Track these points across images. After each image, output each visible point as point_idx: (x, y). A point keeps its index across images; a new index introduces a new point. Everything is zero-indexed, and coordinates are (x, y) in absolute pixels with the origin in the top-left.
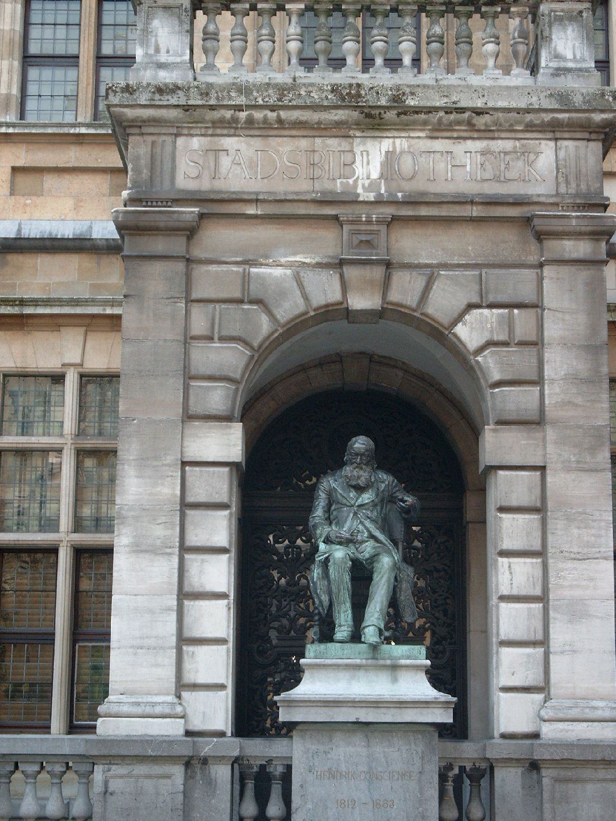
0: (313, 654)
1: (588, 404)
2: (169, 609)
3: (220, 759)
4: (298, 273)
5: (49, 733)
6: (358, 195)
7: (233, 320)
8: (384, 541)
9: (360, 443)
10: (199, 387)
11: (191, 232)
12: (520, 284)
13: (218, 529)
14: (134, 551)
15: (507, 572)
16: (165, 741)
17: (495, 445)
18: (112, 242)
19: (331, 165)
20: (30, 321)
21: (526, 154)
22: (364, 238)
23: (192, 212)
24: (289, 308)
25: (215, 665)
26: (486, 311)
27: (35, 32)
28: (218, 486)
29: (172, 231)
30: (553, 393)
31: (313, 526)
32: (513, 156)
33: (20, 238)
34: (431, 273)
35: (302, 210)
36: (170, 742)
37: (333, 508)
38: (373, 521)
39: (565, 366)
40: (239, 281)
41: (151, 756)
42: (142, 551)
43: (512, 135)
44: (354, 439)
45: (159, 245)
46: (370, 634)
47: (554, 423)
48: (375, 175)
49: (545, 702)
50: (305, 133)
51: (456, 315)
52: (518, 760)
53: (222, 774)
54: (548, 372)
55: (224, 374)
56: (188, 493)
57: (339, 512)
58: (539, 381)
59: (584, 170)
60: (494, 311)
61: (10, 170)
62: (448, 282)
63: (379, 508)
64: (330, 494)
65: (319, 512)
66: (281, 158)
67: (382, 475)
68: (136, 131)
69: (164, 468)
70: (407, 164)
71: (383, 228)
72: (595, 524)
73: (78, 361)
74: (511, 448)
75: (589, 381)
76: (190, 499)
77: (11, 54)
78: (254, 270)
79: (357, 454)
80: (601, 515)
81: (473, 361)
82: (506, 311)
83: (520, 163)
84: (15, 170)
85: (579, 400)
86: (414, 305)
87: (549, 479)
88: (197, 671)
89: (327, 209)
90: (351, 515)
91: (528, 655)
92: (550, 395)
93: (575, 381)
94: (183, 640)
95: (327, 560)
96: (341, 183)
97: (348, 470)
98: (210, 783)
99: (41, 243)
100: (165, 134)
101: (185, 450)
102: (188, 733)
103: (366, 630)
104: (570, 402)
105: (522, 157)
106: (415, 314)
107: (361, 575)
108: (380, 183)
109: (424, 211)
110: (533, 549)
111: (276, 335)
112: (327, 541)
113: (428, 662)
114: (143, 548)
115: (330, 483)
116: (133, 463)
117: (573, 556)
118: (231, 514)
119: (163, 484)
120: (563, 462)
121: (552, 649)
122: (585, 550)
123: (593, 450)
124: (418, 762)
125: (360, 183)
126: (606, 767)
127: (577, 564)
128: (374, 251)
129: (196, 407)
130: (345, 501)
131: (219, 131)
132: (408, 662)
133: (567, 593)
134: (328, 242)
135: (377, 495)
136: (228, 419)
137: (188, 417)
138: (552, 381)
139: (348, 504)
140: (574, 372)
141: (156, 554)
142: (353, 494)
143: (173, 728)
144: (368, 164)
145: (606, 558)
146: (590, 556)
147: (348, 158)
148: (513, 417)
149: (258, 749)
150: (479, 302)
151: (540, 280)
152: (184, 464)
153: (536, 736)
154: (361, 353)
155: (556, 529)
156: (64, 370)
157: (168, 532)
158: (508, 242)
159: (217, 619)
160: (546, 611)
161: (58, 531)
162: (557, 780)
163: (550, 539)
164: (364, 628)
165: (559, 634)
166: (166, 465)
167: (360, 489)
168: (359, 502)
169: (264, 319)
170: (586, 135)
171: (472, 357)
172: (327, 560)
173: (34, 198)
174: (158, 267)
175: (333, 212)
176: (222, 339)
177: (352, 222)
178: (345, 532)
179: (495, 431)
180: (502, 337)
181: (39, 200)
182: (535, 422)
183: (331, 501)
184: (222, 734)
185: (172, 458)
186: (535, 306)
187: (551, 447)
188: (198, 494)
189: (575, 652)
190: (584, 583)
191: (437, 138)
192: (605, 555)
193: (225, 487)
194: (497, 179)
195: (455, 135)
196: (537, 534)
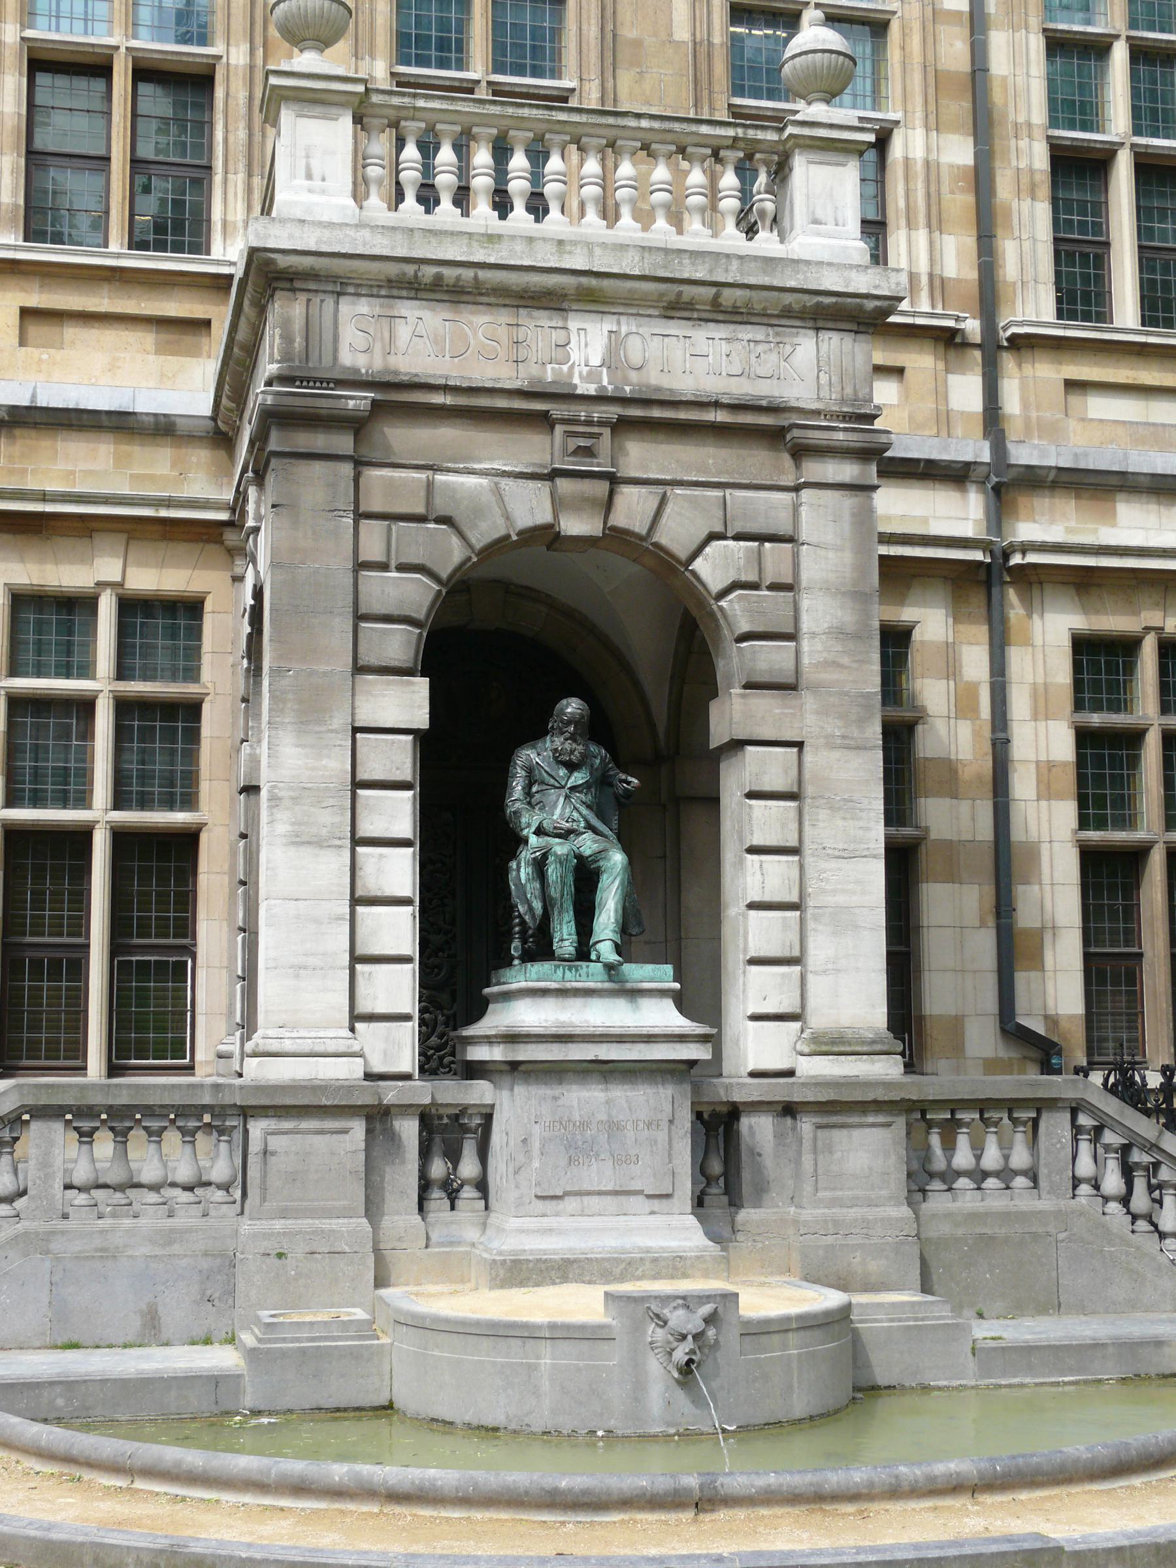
1: (855, 665)
2: (339, 918)
3: (405, 1109)
4: (496, 484)
5: (193, 1075)
6: (576, 386)
7: (418, 542)
9: (572, 707)
12: (771, 508)
13: (397, 813)
14: (293, 843)
15: (758, 873)
16: (342, 1087)
18: (162, 418)
20: (53, 523)
22: (582, 442)
23: (365, 398)
24: (484, 532)
25: (397, 989)
26: (731, 543)
28: (396, 758)
30: (812, 650)
31: (515, 812)
33: (36, 408)
35: (502, 403)
36: (348, 1088)
37: (534, 789)
38: (588, 807)
39: (828, 618)
40: (423, 493)
41: (325, 1106)
43: (765, 320)
44: (564, 702)
45: (320, 441)
46: (606, 951)
47: (815, 688)
48: (596, 361)
49: (802, 1031)
50: (501, 301)
51: (694, 546)
52: (770, 1103)
53: (409, 1130)
54: (806, 624)
55: (403, 613)
56: (359, 769)
60: (742, 543)
64: (530, 770)
69: (330, 735)
71: (607, 432)
72: (864, 814)
73: (118, 579)
74: (763, 718)
75: (857, 637)
76: (362, 775)
78: (440, 477)
80: (870, 803)
81: (714, 607)
82: (756, 544)
83: (773, 357)
84: (27, 313)
85: (845, 660)
86: (644, 532)
88: (375, 998)
89: (530, 409)
90: (562, 799)
91: (783, 975)
92: (811, 652)
93: (841, 636)
96: (553, 369)
98: (393, 1138)
100: (324, 292)
102: (369, 1076)
103: (599, 946)
104: (834, 662)
105: (776, 350)
107: (586, 876)
108: (601, 373)
109: (656, 413)
110: (788, 844)
112: (539, 832)
114: (305, 838)
115: (529, 755)
116: (290, 727)
117: (837, 853)
118: (414, 795)
119: (329, 757)
120: (826, 737)
122: (852, 847)
123: (861, 722)
124: (668, 1108)
125: (577, 369)
127: (842, 863)
128: (595, 461)
129: (369, 657)
130: (552, 781)
131: (395, 292)
133: (830, 900)
134: (534, 449)
135: (591, 774)
137: (359, 669)
138: (814, 635)
139: (557, 784)
141: (321, 847)
142: (562, 772)
143: (348, 1070)
145: (875, 857)
146: (857, 853)
148: (766, 678)
149: (452, 1092)
150: (723, 530)
151: (796, 508)
152: (356, 730)
153: (790, 1073)
154: (496, 581)
155: (818, 820)
156: (97, 590)
157: (337, 819)
158: (757, 461)
160: (802, 921)
161: (89, 807)
165: (819, 950)
166: (332, 731)
167: (572, 767)
169: (455, 540)
171: (712, 602)
173: (52, 351)
174: (318, 468)
176: (402, 568)
177: (565, 421)
179: (743, 696)
180: (752, 577)
181: (58, 355)
184: (407, 1077)
185: (340, 720)
186: (790, 540)
187: (805, 717)
188: (371, 770)
189: (838, 971)
190: (850, 887)
191: (673, 318)
192: (875, 852)
195: (695, 315)
196: (794, 826)
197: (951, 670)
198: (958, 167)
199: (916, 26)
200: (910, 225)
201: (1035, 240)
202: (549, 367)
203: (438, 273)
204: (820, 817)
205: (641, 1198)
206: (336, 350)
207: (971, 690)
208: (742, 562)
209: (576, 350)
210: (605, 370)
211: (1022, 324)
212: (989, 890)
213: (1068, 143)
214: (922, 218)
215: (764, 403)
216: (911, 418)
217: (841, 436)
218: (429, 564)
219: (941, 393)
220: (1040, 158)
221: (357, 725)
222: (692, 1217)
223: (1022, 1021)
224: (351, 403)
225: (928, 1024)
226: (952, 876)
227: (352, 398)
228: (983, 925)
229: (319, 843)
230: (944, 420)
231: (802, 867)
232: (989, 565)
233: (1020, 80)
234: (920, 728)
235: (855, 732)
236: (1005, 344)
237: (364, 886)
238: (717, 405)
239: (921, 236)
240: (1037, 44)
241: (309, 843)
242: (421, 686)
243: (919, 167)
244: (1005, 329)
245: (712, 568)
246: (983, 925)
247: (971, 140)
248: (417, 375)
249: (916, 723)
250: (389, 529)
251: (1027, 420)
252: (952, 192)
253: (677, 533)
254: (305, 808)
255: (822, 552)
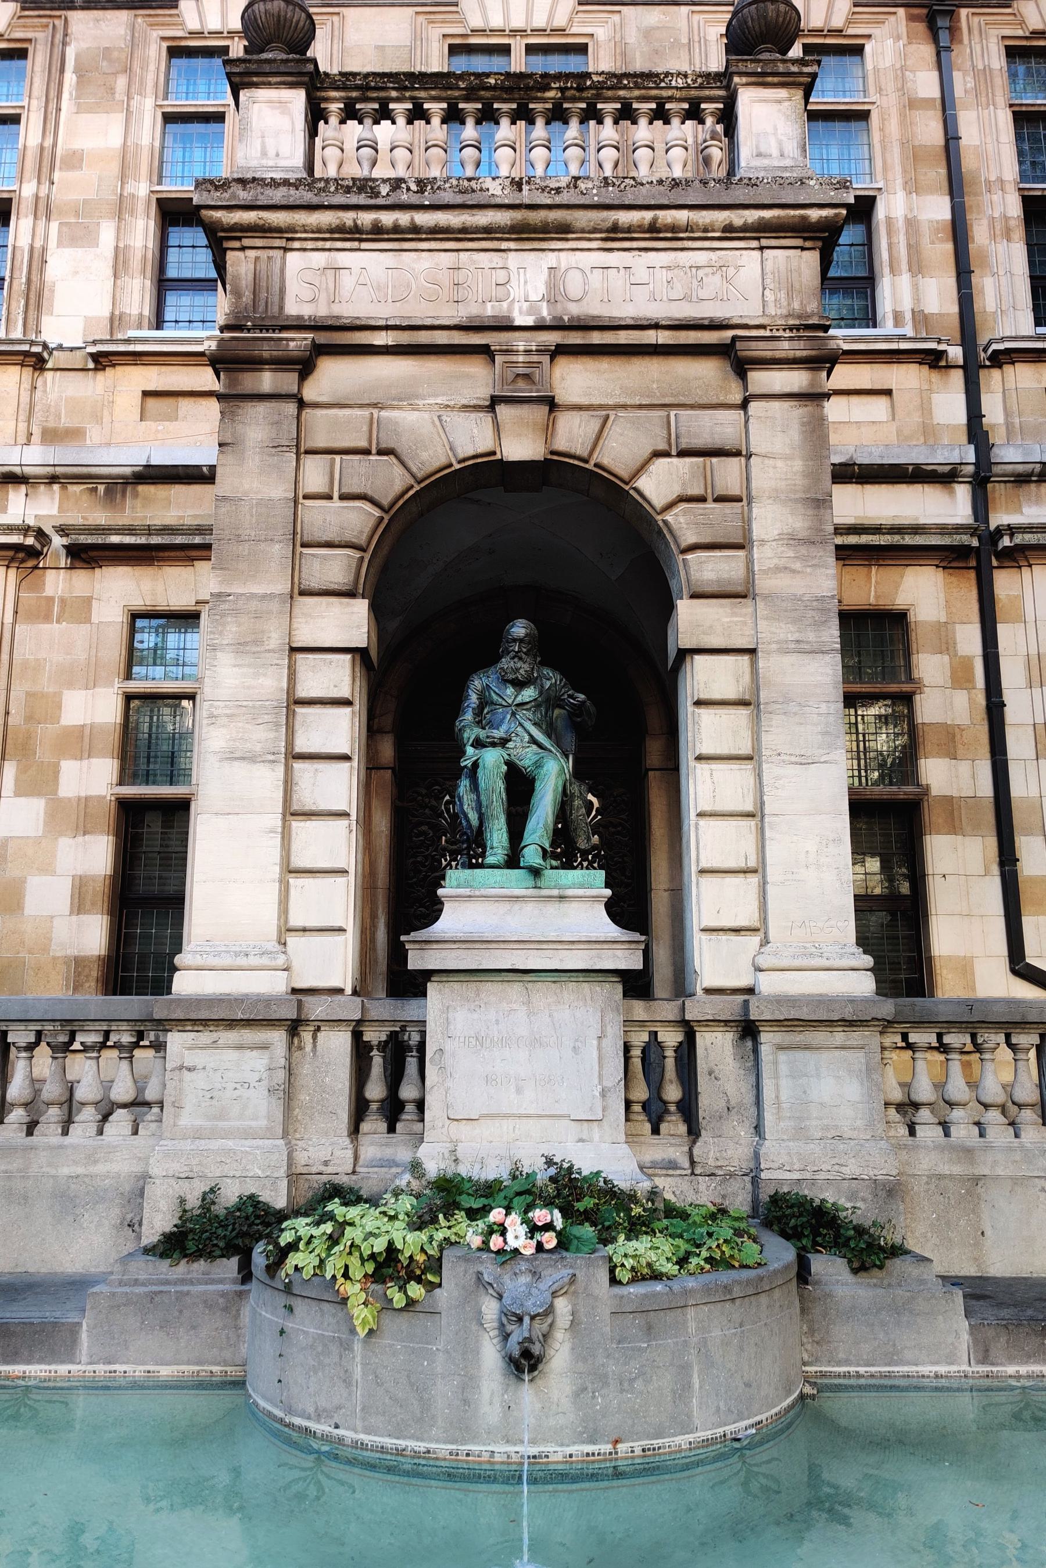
0: (456, 882)
7: (360, 473)
8: (549, 747)
10: (313, 555)
11: (305, 367)
13: (339, 730)
15: (709, 781)
17: (692, 621)
19: (480, 286)
21: (724, 269)
23: (305, 339)
25: (335, 902)
26: (675, 460)
27: (173, 255)
28: (337, 677)
29: (281, 363)
30: (764, 556)
31: (460, 730)
32: (709, 270)
34: (604, 413)
36: (267, 1001)
42: (236, 759)
45: (267, 381)
46: (531, 855)
52: (726, 1022)
53: (337, 1044)
54: (757, 532)
57: (494, 714)
58: (741, 545)
59: (797, 286)
61: (140, 394)
62: (629, 425)
63: (543, 710)
65: (469, 716)
66: (416, 278)
67: (546, 671)
68: (236, 244)
69: (267, 655)
70: (574, 285)
71: (546, 359)
77: (144, 272)
79: (514, 640)
82: (701, 459)
83: (717, 278)
85: (797, 566)
87: (761, 664)
89: (474, 340)
90: (509, 716)
93: (791, 542)
94: (290, 872)
95: (475, 765)
96: (492, 306)
97: (506, 663)
99: (174, 472)
101: (293, 633)
103: (526, 850)
104: (786, 568)
106: (587, 466)
107: (520, 786)
109: (596, 338)
111: (411, 493)
113: (608, 892)
117: (793, 759)
119: (265, 675)
121: (769, 879)
125: (516, 305)
126: (846, 1029)
128: (534, 388)
132: (580, 892)
134: (475, 379)
135: (541, 693)
136: (351, 594)
140: (790, 531)
142: (510, 690)
143: (270, 984)
144: (524, 284)
146: (816, 759)
147: (501, 276)
153: (750, 991)
155: (772, 726)
156: (198, 608)
158: (706, 373)
159: (335, 844)
160: (761, 831)
162: (781, 1048)
163: (765, 738)
164: (525, 846)
166: (269, 651)
167: (519, 685)
168: (519, 699)
169: (398, 470)
170: (799, 242)
172: (475, 765)
174: (261, 409)
175: (483, 342)
176: (343, 497)
178: (498, 734)
180: (696, 490)
182: (738, 594)
183: (484, 702)
185: (275, 639)
186: (738, 454)
188: (310, 686)
193: (347, 680)
194: (686, 298)
197: (946, 645)
198: (937, 222)
199: (894, 113)
200: (893, 271)
201: (1012, 275)
202: (489, 305)
203: (376, 220)
204: (774, 723)
205: (566, 1122)
206: (282, 299)
207: (966, 663)
208: (687, 477)
209: (516, 288)
210: (545, 304)
211: (1002, 340)
212: (992, 842)
213: (1039, 193)
214: (904, 266)
215: (706, 322)
216: (899, 432)
217: (786, 345)
218: (370, 493)
219: (925, 408)
220: (1014, 208)
221: (294, 645)
222: (625, 1146)
223: (1028, 960)
224: (292, 344)
225: (937, 964)
226: (954, 828)
227: (293, 340)
228: (987, 873)
229: (251, 758)
230: (929, 431)
231: (759, 776)
232: (978, 548)
233: (990, 147)
234: (917, 697)
235: (811, 636)
236: (988, 363)
237: (299, 800)
238: (656, 326)
239: (905, 279)
240: (1005, 120)
241: (243, 758)
242: (361, 607)
243: (901, 224)
244: (985, 350)
245: (658, 484)
246: (987, 873)
247: (947, 199)
248: (358, 318)
249: (914, 693)
250: (333, 461)
251: (1009, 425)
252: (932, 243)
253: (618, 451)
254: (240, 725)
255: (771, 462)
